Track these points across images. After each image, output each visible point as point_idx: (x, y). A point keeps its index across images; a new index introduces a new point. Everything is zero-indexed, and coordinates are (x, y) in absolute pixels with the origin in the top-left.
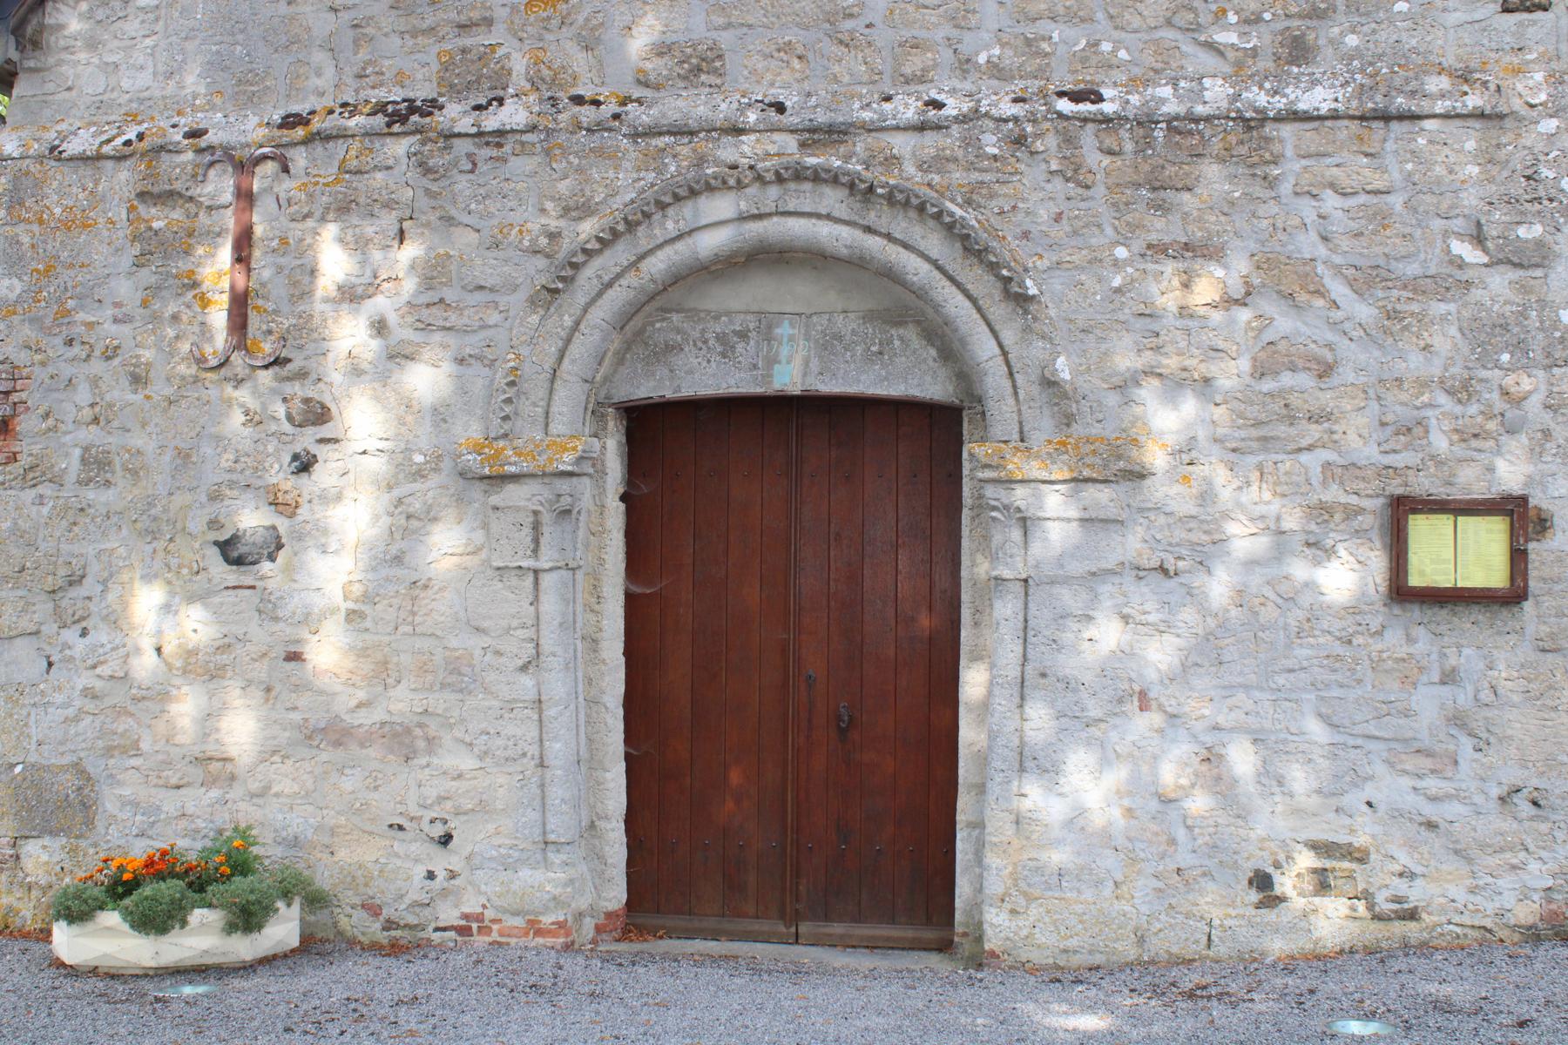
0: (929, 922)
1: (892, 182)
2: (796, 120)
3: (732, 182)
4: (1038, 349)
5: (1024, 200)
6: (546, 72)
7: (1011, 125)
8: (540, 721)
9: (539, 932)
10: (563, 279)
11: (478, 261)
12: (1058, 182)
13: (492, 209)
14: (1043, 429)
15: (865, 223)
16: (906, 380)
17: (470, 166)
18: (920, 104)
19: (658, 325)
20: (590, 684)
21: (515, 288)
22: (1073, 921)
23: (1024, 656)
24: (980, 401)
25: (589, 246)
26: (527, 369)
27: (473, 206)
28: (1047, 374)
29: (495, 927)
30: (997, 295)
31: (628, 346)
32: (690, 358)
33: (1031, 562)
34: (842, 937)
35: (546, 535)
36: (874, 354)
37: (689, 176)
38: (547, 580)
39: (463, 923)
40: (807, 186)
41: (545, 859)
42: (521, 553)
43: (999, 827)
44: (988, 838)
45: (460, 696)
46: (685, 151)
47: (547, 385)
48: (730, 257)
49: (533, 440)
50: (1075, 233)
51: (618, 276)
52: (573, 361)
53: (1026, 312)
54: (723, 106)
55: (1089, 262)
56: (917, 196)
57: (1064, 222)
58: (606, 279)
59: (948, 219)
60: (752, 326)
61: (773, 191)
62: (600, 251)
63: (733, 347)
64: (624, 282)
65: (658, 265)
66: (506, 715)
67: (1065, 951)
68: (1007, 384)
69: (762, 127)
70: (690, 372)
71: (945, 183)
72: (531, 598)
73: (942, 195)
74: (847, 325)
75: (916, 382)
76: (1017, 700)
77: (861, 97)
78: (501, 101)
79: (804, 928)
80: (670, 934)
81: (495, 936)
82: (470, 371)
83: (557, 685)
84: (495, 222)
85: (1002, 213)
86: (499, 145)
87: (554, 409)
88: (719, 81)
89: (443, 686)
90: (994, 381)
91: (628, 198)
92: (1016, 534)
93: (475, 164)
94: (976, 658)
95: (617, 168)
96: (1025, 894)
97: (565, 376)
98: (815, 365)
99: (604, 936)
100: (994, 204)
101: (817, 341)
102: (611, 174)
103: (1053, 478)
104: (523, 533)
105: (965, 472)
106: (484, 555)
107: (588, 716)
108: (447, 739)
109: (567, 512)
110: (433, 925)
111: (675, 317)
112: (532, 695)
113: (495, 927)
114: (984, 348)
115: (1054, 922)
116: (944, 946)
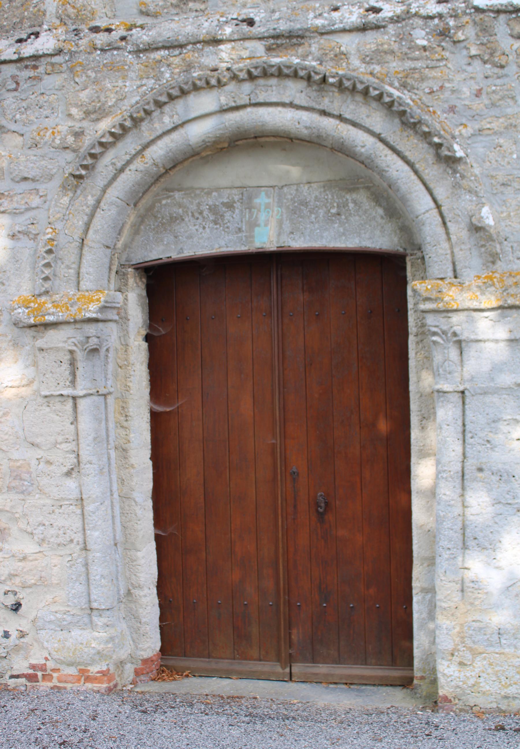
0: (393, 663)
1: (341, 72)
2: (262, 30)
3: (213, 82)
4: (466, 202)
5: (449, 81)
6: (71, 11)
7: (436, 21)
8: (83, 514)
9: (88, 679)
10: (85, 167)
11: (23, 159)
12: (477, 63)
13: (32, 118)
14: (472, 265)
15: (321, 107)
16: (359, 235)
17: (14, 86)
18: (362, 11)
19: (164, 202)
20: (123, 484)
21: (51, 177)
22: (511, 672)
23: (464, 455)
24: (420, 249)
25: (104, 140)
26: (62, 240)
27: (18, 116)
28: (474, 220)
29: (55, 675)
30: (430, 158)
31: (142, 219)
32: (190, 226)
33: (466, 376)
34: (326, 675)
35: (81, 369)
36: (334, 215)
37: (180, 79)
38: (82, 404)
39: (31, 671)
40: (273, 81)
41: (91, 622)
42: (62, 384)
43: (447, 592)
44: (438, 604)
45: (21, 496)
46: (176, 61)
47: (76, 251)
48: (215, 142)
49: (67, 295)
50: (493, 105)
51: (129, 163)
52: (96, 231)
53: (455, 171)
54: (206, 24)
55: (506, 128)
56: (362, 82)
57: (484, 96)
58: (119, 165)
59: (387, 99)
60: (236, 198)
61: (247, 87)
62: (113, 144)
63: (222, 216)
64: (132, 167)
65: (159, 151)
66: (57, 511)
67: (506, 697)
68: (441, 230)
69: (236, 37)
70: (190, 237)
71: (384, 72)
72: (71, 419)
73: (382, 81)
74: (311, 193)
75: (367, 236)
76: (459, 491)
77: (314, 9)
78: (37, 35)
79: (297, 668)
80: (195, 673)
81: (55, 682)
82: (19, 244)
83: (94, 486)
84: (34, 127)
85: (432, 92)
86: (35, 67)
87: (83, 270)
88: (203, 7)
89: (10, 489)
90: (430, 229)
91: (133, 101)
92: (453, 353)
93: (17, 83)
94: (424, 454)
95: (124, 78)
96: (471, 649)
97: (90, 244)
98: (287, 226)
99: (142, 678)
100: (425, 86)
101: (288, 208)
102: (120, 83)
103: (482, 306)
104: (63, 368)
105: (410, 306)
106: (35, 386)
107: (122, 508)
108: (14, 530)
109: (95, 351)
110: (9, 673)
111: (177, 195)
112: (75, 494)
113: (55, 675)
114: (421, 203)
115: (496, 673)
116: (406, 683)
